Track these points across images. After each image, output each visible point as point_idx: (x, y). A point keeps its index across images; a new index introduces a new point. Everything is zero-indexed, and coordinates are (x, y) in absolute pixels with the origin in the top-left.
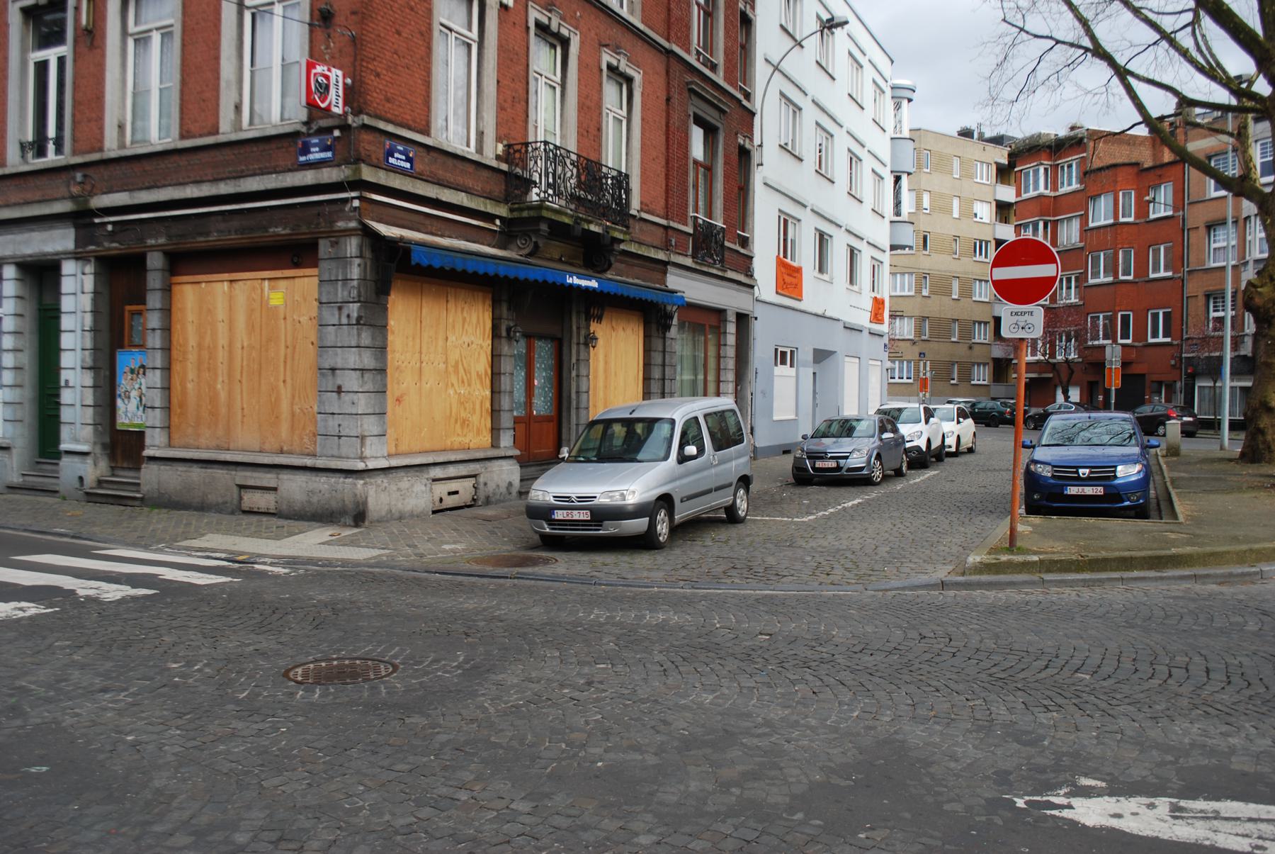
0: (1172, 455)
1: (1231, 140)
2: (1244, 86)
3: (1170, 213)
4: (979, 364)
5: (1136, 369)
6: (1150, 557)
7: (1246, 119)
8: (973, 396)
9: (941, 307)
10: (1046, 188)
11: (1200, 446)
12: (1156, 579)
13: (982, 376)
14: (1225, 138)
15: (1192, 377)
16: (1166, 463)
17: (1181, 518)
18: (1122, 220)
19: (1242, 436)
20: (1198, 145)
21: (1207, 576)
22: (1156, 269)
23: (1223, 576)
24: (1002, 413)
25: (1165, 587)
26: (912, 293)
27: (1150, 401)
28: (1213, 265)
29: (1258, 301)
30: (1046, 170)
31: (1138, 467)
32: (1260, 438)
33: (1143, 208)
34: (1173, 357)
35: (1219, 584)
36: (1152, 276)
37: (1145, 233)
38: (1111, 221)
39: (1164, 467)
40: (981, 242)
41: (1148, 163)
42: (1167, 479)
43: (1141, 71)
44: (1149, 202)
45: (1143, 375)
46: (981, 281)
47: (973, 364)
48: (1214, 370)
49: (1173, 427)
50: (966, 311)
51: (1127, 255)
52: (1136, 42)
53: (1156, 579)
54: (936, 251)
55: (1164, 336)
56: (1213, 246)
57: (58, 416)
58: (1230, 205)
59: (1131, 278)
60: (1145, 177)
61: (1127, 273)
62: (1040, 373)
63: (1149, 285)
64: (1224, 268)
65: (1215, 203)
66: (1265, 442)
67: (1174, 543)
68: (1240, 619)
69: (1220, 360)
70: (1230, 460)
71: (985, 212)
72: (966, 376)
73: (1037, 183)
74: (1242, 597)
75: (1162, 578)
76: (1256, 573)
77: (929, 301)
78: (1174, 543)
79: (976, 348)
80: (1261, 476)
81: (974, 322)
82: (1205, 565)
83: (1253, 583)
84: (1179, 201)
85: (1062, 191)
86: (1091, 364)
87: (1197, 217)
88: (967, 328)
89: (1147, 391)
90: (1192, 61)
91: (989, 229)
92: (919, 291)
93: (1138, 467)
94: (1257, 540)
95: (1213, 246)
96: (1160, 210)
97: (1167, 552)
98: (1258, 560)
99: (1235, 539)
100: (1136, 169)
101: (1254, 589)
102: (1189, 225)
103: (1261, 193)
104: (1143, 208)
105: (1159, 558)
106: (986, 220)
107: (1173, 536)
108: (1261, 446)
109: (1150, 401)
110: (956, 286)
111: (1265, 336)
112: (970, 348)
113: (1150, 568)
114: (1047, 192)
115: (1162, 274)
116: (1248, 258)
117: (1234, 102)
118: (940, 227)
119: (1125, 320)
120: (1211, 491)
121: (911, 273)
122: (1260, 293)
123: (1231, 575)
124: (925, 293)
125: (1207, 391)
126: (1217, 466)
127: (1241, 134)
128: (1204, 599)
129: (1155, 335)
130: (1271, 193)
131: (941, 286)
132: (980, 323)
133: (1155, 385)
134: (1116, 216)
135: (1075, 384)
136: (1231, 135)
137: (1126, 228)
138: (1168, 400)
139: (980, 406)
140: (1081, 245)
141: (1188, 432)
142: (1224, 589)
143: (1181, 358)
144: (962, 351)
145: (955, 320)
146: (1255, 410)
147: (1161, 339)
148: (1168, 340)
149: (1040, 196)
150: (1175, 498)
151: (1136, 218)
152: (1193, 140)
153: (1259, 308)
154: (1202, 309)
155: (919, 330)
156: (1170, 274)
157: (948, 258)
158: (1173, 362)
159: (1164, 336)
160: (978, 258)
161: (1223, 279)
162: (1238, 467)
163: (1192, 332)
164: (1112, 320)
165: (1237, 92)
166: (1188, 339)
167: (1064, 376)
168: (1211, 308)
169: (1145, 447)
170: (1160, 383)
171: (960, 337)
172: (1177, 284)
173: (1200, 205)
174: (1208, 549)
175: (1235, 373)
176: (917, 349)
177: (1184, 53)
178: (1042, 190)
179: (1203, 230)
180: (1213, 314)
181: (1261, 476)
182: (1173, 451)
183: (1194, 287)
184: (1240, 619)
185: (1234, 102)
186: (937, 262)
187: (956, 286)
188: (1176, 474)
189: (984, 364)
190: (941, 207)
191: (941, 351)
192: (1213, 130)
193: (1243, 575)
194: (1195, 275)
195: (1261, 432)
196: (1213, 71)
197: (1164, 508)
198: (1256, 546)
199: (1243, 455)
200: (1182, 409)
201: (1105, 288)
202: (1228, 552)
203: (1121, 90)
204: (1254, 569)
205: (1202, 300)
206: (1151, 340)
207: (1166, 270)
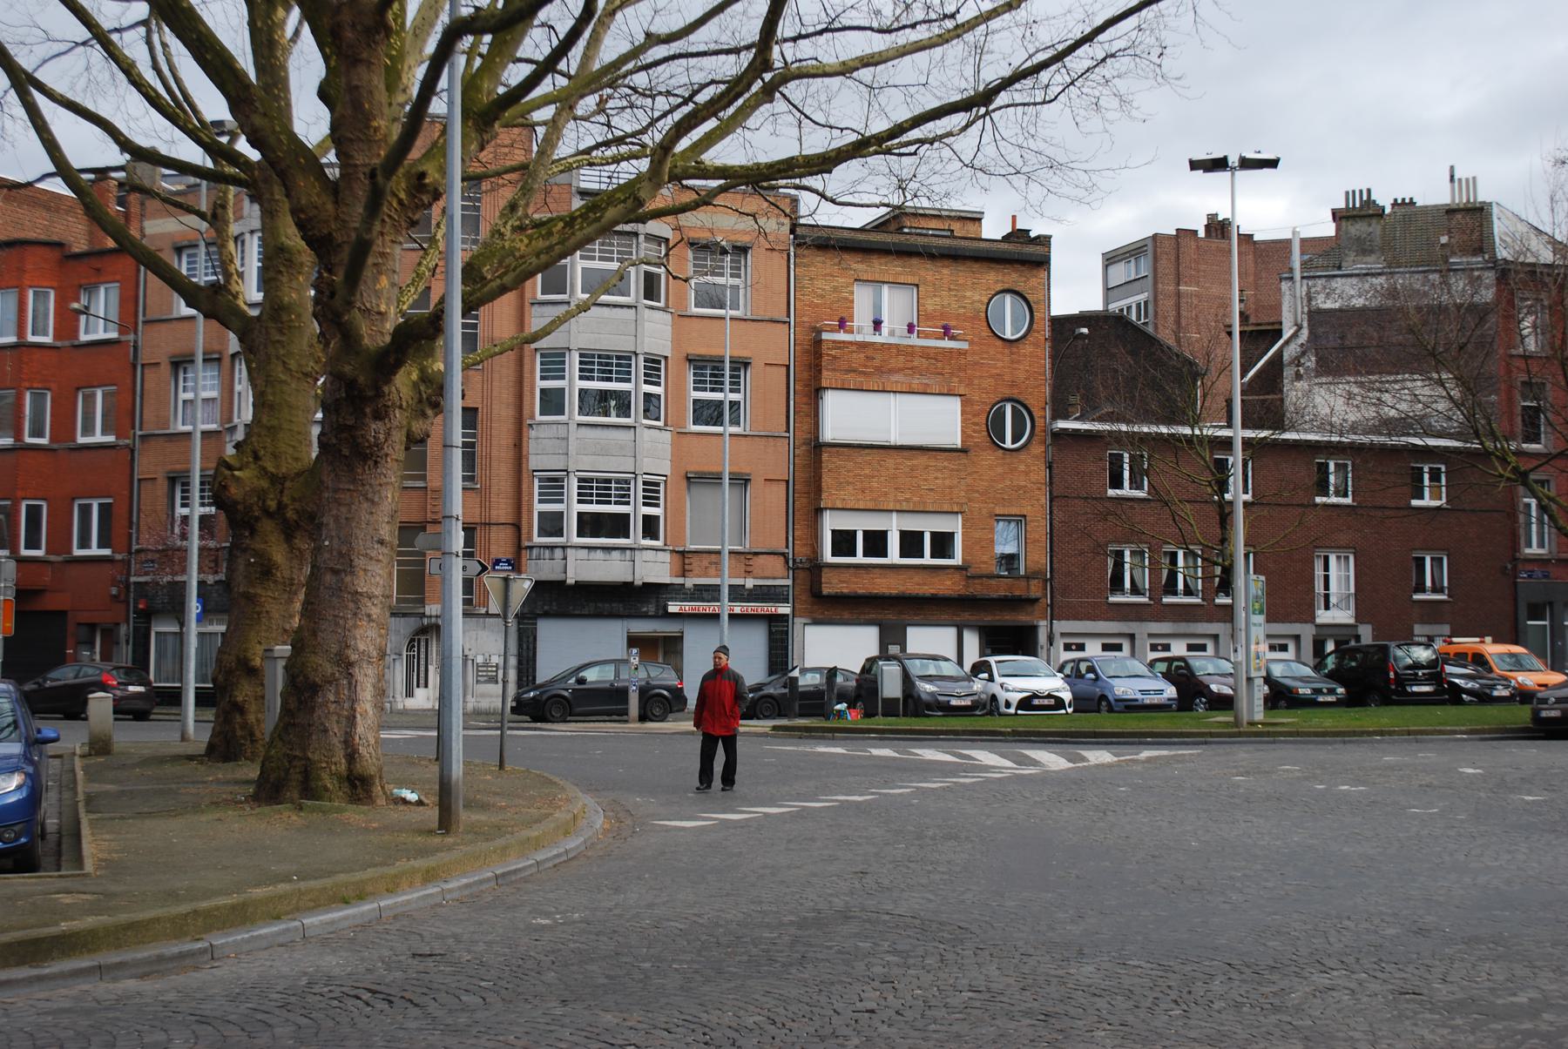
0: (98, 754)
1: (204, 225)
2: (224, 140)
3: (114, 335)
5: (50, 603)
6: (21, 943)
7: (225, 193)
11: (132, 738)
12: (30, 981)
14: (193, 220)
15: (147, 616)
16: (85, 769)
17: (89, 866)
18: (31, 338)
19: (210, 714)
20: (159, 228)
21: (121, 965)
22: (88, 429)
23: (147, 962)
25: (42, 995)
27: (75, 659)
29: (235, 492)
31: (16, 780)
32: (238, 719)
33: (67, 321)
34: (114, 583)
35: (142, 977)
36: (81, 440)
37: (71, 365)
38: (12, 339)
39: (80, 774)
41: (80, 246)
42: (81, 797)
43: (60, 87)
44: (79, 312)
45: (63, 613)
48: (177, 610)
49: (100, 704)
51: (1437, 562)
52: (57, 34)
53: (30, 981)
55: (100, 546)
56: (183, 396)
58: (202, 333)
59: (44, 441)
60: (73, 270)
61: (32, 543)
64: (189, 434)
66: (245, 725)
67: (65, 913)
68: (161, 1037)
69: (183, 586)
70: (191, 758)
74: (171, 996)
75: (40, 979)
76: (203, 951)
78: (65, 913)
80: (237, 782)
82: (118, 947)
83: (197, 968)
84: (129, 316)
87: (157, 345)
90: (137, 82)
93: (16, 780)
94: (207, 894)
95: (183, 396)
96: (96, 330)
97: (53, 930)
98: (208, 929)
99: (173, 896)
100: (53, 255)
101: (193, 979)
102: (144, 357)
103: (243, 315)
104: (67, 321)
105: (36, 942)
107: (67, 899)
108: (239, 733)
109: (75, 659)
111: (245, 550)
113: (21, 963)
115: (98, 438)
116: (236, 420)
117: (209, 164)
119: (34, 513)
120: (150, 815)
122: (238, 479)
123: (161, 959)
125: (170, 639)
126: (168, 769)
127: (216, 217)
128: (107, 1009)
129: (85, 543)
130: (258, 318)
136: (202, 216)
138: (106, 657)
141: (128, 711)
142: (148, 986)
143: (128, 585)
146: (230, 672)
147: (94, 551)
148: (107, 552)
150: (86, 831)
151: (56, 337)
152: (154, 216)
153: (236, 503)
154: (162, 502)
156: (111, 439)
158: (114, 591)
159: (100, 546)
161: (188, 452)
162: (202, 768)
163: (146, 540)
165: (211, 148)
166: (138, 551)
168: (178, 501)
169: (35, 743)
170: (92, 627)
173: (163, 327)
174: (123, 918)
175: (206, 614)
177: (128, 70)
179: (165, 369)
181: (237, 782)
182: (100, 746)
183: (149, 464)
184: (161, 1037)
185: (209, 164)
188: (96, 787)
192: (175, 204)
193: (182, 956)
195: (240, 709)
196: (178, 111)
197: (68, 846)
198: (204, 905)
199: (211, 748)
200: (128, 672)
202: (158, 920)
203: (20, 112)
204: (199, 945)
205: (163, 485)
206: (77, 552)
207: (104, 432)
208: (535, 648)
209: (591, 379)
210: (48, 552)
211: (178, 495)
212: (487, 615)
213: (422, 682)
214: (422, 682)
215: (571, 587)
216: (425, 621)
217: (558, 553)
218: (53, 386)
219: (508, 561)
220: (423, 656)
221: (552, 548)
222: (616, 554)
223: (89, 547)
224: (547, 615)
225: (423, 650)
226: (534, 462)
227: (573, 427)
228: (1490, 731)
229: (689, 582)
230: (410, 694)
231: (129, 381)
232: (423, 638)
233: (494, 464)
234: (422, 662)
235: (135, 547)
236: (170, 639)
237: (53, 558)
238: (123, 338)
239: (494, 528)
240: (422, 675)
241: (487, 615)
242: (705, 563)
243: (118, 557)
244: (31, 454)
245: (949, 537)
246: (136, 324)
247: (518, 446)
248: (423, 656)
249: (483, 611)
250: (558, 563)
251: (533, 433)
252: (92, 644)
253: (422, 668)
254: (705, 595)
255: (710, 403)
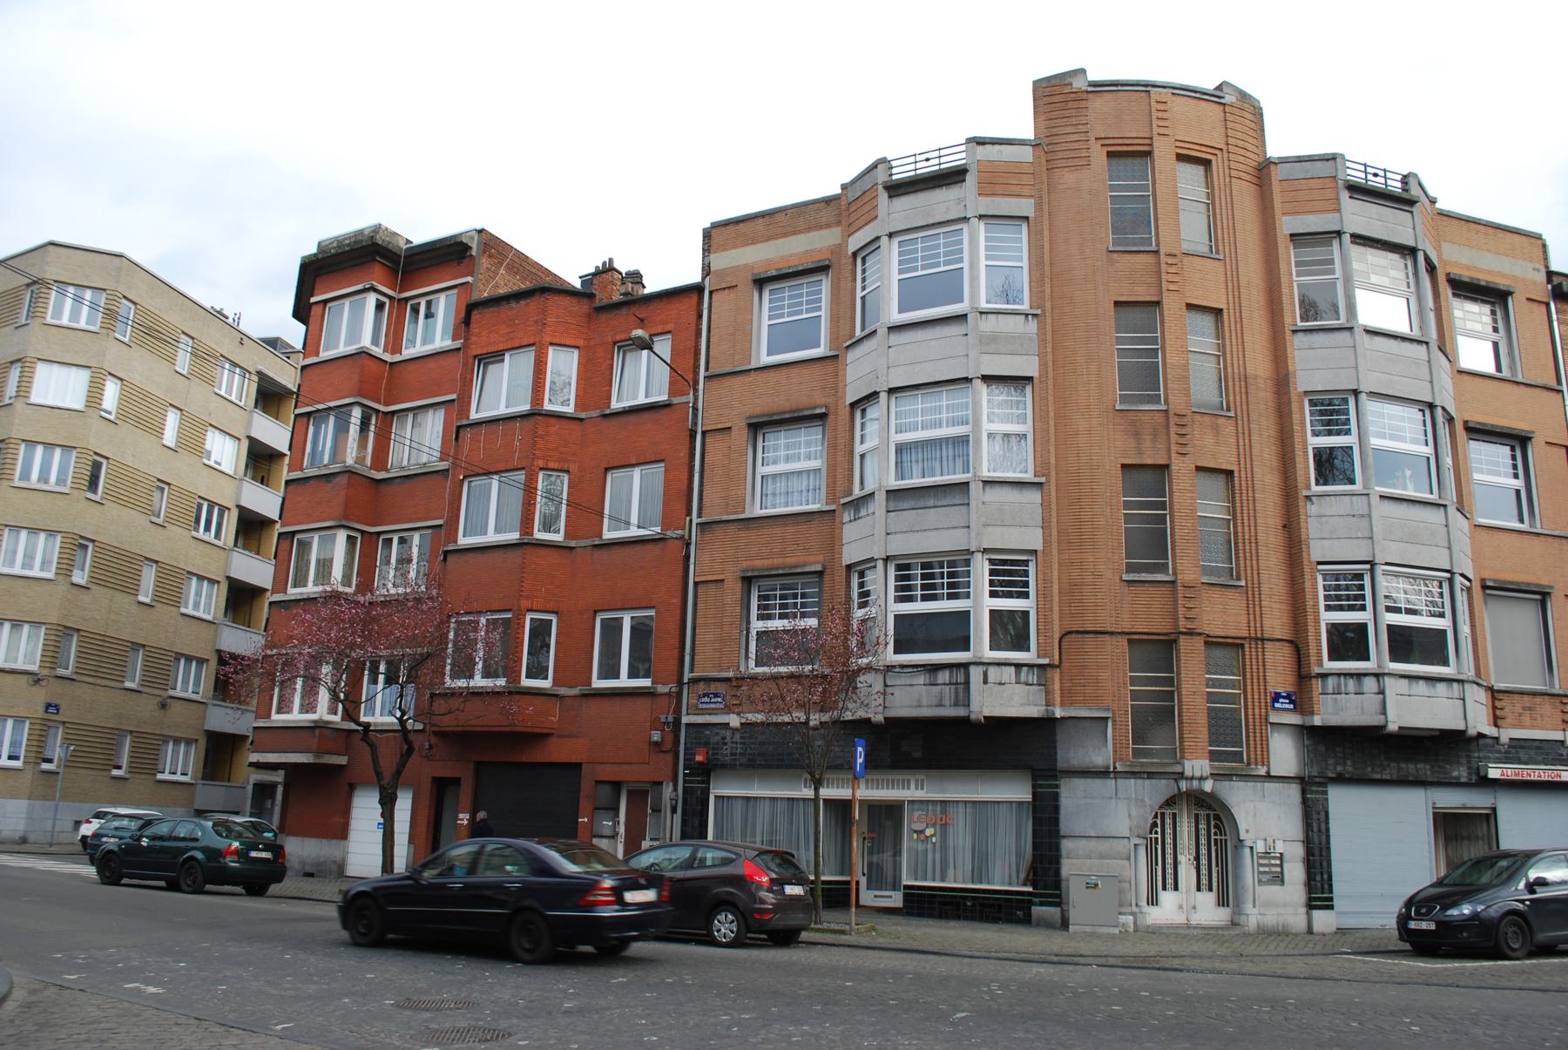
4: (177, 741)
8: (150, 805)
9: (107, 614)
10: (375, 342)
13: (180, 765)
15: (703, 773)
24: (214, 854)
26: (50, 575)
28: (758, 512)
30: (380, 306)
40: (212, 504)
46: (201, 578)
47: (165, 739)
50: (160, 631)
54: (118, 500)
56: (762, 470)
57: (1057, 848)
62: (319, 752)
63: (604, 553)
65: (772, 376)
71: (225, 453)
72: (146, 762)
73: (356, 325)
77: (85, 597)
79: (176, 707)
81: (178, 657)
85: (408, 352)
86: (460, 740)
88: (161, 665)
89: (585, 805)
91: (230, 486)
92: (65, 570)
95: (762, 470)
104: (595, 381)
106: (227, 467)
110: (149, 577)
112: (163, 706)
114: (378, 351)
118: (131, 452)
119: (540, 630)
121: (51, 533)
124: (79, 577)
125: (738, 808)
129: (611, 671)
131: (117, 570)
132: (189, 659)
133: (606, 791)
134: (526, 524)
135: (407, 785)
137: (556, 426)
139: (163, 829)
140: (444, 465)
144: (145, 709)
145: (136, 646)
147: (624, 681)
148: (645, 682)
149: (363, 353)
155: (53, 655)
157: (142, 520)
158: (656, 736)
160: (201, 533)
164: (510, 629)
167: (388, 763)
170: (616, 786)
171: (144, 682)
172: (667, 549)
173: (736, 382)
176: (40, 696)
178: (366, 341)
179: (740, 434)
180: (757, 625)
186: (118, 525)
187: (149, 577)
189: (189, 742)
190: (141, 412)
191: (93, 704)
194: (719, 532)
201: (498, 556)
205: (734, 589)
208: (1328, 830)
209: (910, 599)
210: (555, 683)
211: (754, 603)
212: (1269, 777)
213: (1170, 881)
214: (1170, 881)
215: (1392, 736)
216: (1184, 785)
217: (1370, 684)
218: (573, 467)
219: (1288, 697)
220: (1169, 840)
221: (1359, 676)
222: (1441, 687)
223: (617, 676)
224: (1341, 780)
225: (1169, 831)
226: (1318, 550)
227: (1375, 500)
228: (844, 837)
229: (1506, 735)
230: (1153, 900)
231: (684, 453)
232: (1168, 812)
233: (1262, 551)
234: (1169, 850)
235: (687, 676)
236: (738, 808)
237: (563, 691)
238: (676, 400)
239: (1268, 645)
240: (1170, 870)
241: (1269, 777)
242: (1518, 708)
243: (662, 689)
244: (542, 552)
245: (1279, 879)
246: (696, 382)
247: (1291, 529)
248: (1169, 840)
249: (1262, 771)
250: (1370, 700)
251: (1312, 509)
252: (616, 810)
253: (1169, 860)
254: (1522, 754)
255: (1012, 613)
